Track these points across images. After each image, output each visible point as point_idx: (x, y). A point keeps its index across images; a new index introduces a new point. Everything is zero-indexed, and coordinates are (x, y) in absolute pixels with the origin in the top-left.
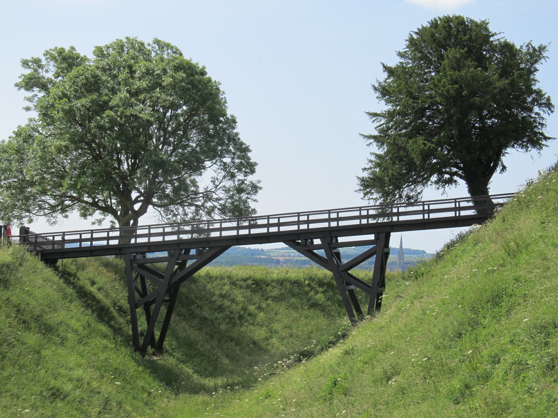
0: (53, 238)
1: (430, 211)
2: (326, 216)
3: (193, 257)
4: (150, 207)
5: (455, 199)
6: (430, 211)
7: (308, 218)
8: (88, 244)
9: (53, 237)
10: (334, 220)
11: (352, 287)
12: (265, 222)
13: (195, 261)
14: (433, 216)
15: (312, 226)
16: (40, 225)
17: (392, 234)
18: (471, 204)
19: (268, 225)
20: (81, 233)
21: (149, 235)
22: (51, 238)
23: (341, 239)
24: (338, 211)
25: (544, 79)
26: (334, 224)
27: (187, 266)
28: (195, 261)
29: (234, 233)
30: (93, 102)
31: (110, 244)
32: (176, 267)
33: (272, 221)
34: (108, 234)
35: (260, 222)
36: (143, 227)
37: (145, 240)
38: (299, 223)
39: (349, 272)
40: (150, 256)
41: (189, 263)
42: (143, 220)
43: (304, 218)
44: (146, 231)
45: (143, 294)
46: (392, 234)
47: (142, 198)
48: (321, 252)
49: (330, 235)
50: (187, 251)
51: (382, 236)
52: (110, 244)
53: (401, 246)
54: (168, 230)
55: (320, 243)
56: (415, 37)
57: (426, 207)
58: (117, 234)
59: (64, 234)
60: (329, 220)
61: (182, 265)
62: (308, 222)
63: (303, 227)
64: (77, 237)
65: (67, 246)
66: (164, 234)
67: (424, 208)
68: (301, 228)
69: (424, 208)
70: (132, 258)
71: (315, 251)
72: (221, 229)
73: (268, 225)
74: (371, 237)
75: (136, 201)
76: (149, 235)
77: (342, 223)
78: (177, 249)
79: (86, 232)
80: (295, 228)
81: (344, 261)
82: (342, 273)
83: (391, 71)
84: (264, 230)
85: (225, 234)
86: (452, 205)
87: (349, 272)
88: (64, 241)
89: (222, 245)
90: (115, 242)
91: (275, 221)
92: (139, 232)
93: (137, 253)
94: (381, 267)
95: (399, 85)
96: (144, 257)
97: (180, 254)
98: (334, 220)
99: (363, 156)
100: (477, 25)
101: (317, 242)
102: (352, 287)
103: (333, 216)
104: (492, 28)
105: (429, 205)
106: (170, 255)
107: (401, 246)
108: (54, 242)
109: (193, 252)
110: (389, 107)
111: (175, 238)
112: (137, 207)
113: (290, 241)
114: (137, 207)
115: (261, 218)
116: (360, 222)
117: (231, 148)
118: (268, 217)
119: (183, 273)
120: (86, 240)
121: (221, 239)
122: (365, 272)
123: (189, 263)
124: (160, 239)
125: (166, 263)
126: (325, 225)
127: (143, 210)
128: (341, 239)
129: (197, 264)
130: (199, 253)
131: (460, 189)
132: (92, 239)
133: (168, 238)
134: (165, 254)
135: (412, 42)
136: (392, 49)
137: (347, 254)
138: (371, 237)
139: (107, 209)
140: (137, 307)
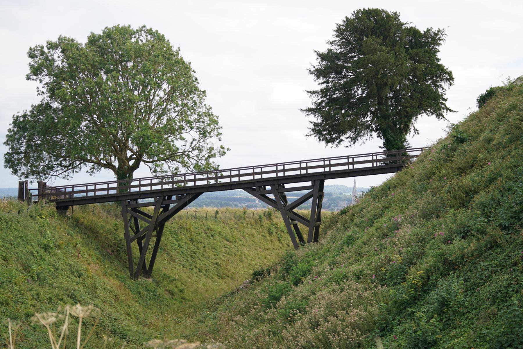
0: (65, 190)
2: (274, 168)
3: (174, 202)
4: (142, 163)
5: (372, 154)
6: (353, 163)
7: (151, 182)
8: (92, 194)
9: (65, 188)
10: (281, 171)
11: (296, 222)
12: (228, 174)
13: (175, 204)
14: (357, 166)
15: (265, 176)
16: (55, 181)
17: (325, 180)
19: (231, 176)
20: (87, 185)
21: (140, 186)
22: (64, 190)
23: (287, 186)
24: (307, 162)
25: (445, 56)
26: (281, 174)
27: (170, 208)
28: (175, 204)
29: (204, 183)
31: (331, 170)
32: (161, 210)
33: (233, 173)
34: (108, 186)
35: (225, 174)
36: (136, 180)
37: (137, 189)
38: (253, 174)
39: (295, 210)
40: (140, 201)
41: (172, 206)
42: (136, 174)
43: (258, 170)
44: (137, 183)
45: (137, 231)
46: (325, 180)
47: (134, 156)
48: (272, 196)
49: (278, 183)
50: (170, 197)
51: (318, 183)
52: (331, 170)
53: (355, 186)
54: (154, 181)
55: (311, 185)
57: (375, 158)
58: (115, 185)
59: (73, 186)
60: (300, 169)
61: (166, 208)
62: (261, 173)
63: (258, 177)
64: (84, 188)
65: (76, 195)
66: (151, 185)
67: (373, 158)
68: (241, 180)
69: (373, 158)
70: (127, 204)
72: (195, 180)
73: (231, 176)
74: (309, 184)
75: (131, 158)
76: (140, 186)
77: (287, 174)
78: (162, 196)
79: (91, 184)
80: (251, 178)
81: (289, 203)
82: (289, 212)
84: (227, 180)
85: (198, 183)
87: (295, 210)
88: (74, 192)
89: (195, 193)
90: (114, 192)
91: (236, 173)
92: (133, 183)
93: (131, 200)
94: (318, 206)
95: (330, 65)
96: (137, 202)
97: (164, 199)
98: (281, 171)
100: (388, 16)
101: (268, 188)
102: (296, 222)
104: (402, 20)
105: (376, 156)
106: (156, 201)
107: (355, 186)
108: (65, 193)
109: (174, 197)
111: (159, 187)
112: (131, 163)
113: (248, 188)
114: (131, 163)
115: (225, 170)
116: (254, 177)
117: (398, 88)
118: (230, 170)
119: (167, 213)
120: (91, 191)
121: (196, 188)
122: (305, 210)
123: (172, 206)
124: (148, 188)
125: (153, 207)
126: (274, 175)
127: (136, 166)
128: (287, 186)
129: (178, 207)
130: (179, 199)
132: (95, 190)
133: (155, 188)
134: (152, 200)
135: (340, 32)
136: (324, 37)
137: (291, 197)
138: (309, 184)
139: (109, 165)
140: (132, 240)
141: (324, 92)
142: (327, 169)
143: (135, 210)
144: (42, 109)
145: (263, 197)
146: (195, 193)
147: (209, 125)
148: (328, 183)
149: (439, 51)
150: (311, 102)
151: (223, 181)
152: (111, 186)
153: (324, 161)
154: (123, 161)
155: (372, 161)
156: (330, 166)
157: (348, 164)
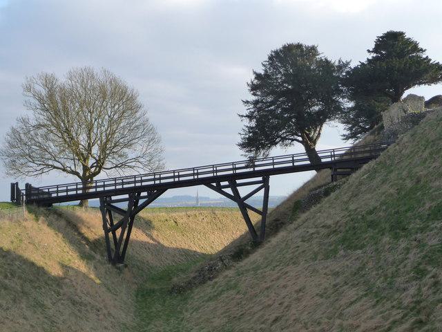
1: (217, 171)
6: (198, 174)
15: (144, 184)
18: (307, 157)
21: (96, 187)
22: (47, 190)
30: (314, 49)
49: (232, 179)
56: (273, 54)
57: (196, 172)
58: (81, 186)
63: (157, 182)
71: (114, 204)
79: (63, 185)
80: (152, 183)
83: (258, 76)
86: (231, 167)
91: (120, 181)
98: (158, 179)
99: (238, 125)
101: (226, 183)
103: (157, 177)
110: (255, 98)
114: (93, 170)
121: (161, 185)
124: (65, 194)
131: (298, 148)
132: (104, 186)
141: (256, 103)
142: (177, 179)
143: (109, 205)
144: (332, 66)
145: (219, 189)
146: (162, 188)
147: (149, 133)
148: (273, 179)
149: (368, 59)
150: (245, 110)
151: (91, 190)
152: (79, 186)
153: (174, 173)
154: (86, 169)
155: (331, 156)
156: (179, 176)
157: (194, 174)
